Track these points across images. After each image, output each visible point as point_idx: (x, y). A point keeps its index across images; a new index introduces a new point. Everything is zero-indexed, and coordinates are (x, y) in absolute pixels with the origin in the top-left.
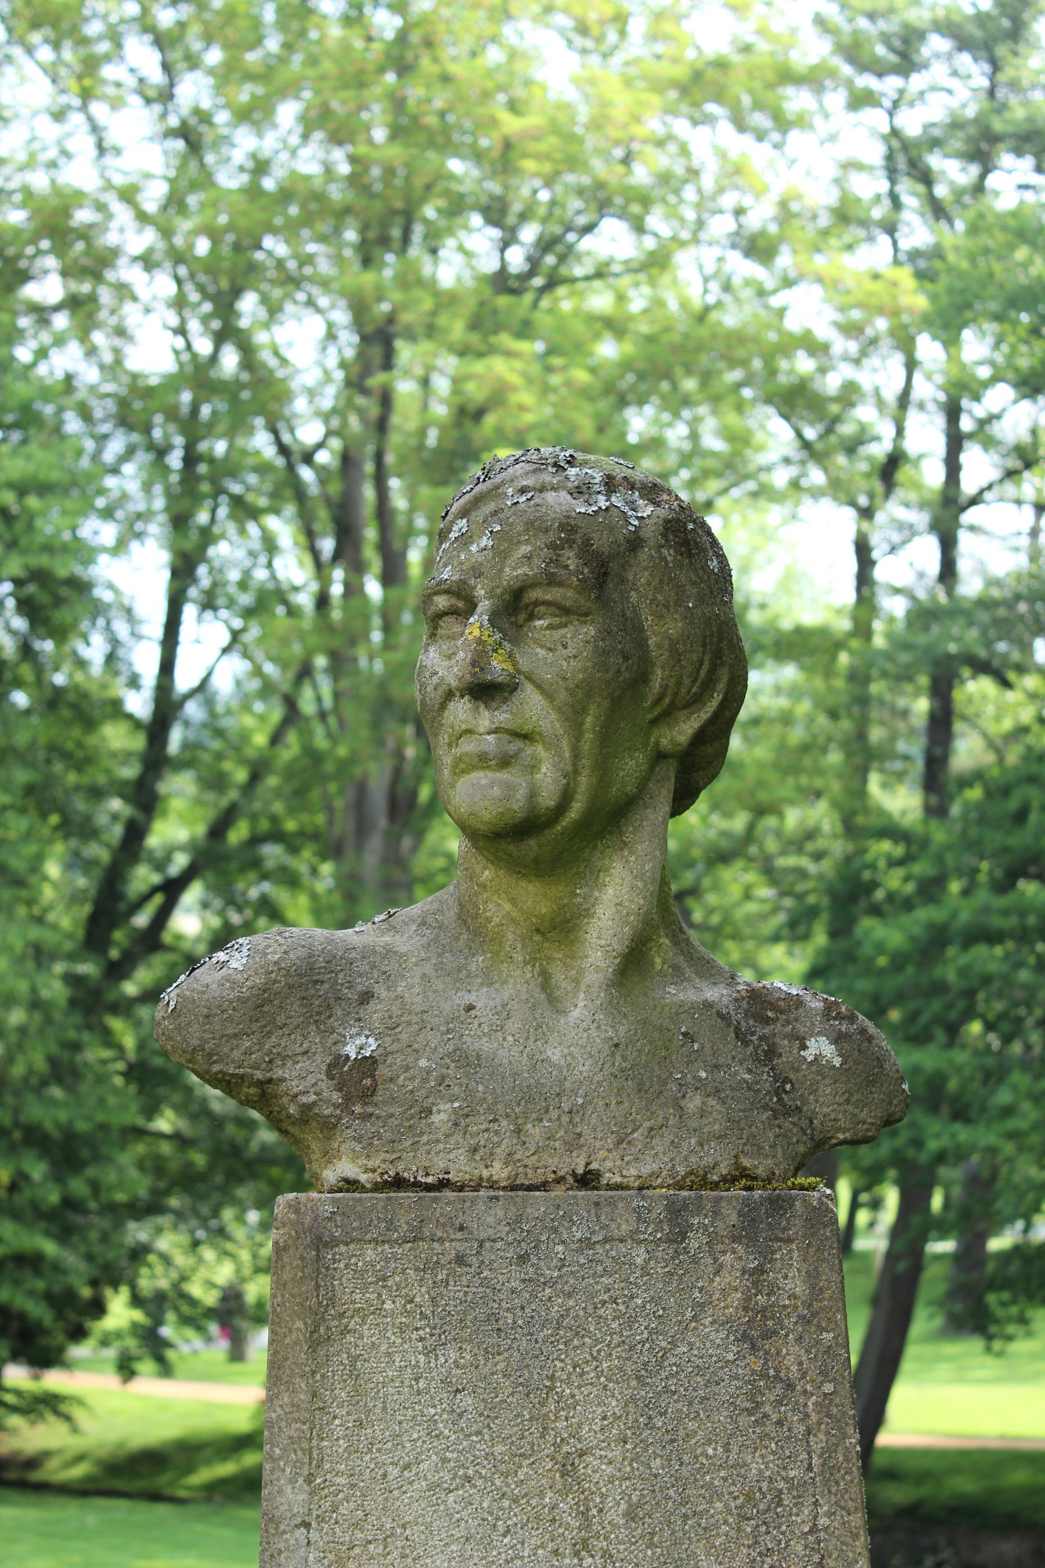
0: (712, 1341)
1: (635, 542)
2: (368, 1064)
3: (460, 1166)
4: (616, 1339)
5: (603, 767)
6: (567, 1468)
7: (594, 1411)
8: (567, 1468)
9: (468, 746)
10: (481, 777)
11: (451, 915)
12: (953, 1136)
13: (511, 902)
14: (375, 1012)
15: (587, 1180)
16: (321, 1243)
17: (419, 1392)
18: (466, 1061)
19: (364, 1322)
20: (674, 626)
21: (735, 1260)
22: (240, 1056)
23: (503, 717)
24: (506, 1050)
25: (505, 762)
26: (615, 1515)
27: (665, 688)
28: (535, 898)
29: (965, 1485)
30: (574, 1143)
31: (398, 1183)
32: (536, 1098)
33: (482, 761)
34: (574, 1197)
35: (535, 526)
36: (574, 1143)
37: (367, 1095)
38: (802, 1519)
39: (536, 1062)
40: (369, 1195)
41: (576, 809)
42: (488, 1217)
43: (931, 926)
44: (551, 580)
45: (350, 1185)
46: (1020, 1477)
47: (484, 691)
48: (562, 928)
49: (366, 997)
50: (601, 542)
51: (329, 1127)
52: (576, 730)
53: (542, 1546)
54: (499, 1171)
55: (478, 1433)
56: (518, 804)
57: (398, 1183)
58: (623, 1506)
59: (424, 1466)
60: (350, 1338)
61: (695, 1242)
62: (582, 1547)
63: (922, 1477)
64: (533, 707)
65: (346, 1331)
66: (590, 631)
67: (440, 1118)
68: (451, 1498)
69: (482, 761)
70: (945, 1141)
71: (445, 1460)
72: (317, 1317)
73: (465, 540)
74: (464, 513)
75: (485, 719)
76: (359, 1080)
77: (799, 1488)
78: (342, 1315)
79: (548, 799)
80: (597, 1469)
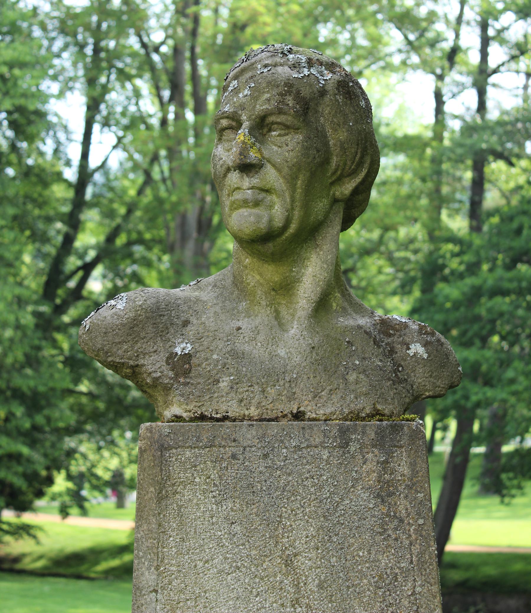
0: (362, 497)
1: (323, 92)
2: (187, 357)
3: (234, 410)
4: (313, 497)
5: (306, 206)
6: (288, 562)
7: (302, 533)
8: (288, 562)
9: (238, 196)
10: (244, 211)
11: (229, 281)
12: (484, 393)
13: (260, 275)
14: (191, 331)
15: (298, 416)
16: (163, 448)
17: (213, 524)
18: (237, 356)
19: (185, 488)
20: (343, 135)
21: (373, 456)
22: (121, 353)
23: (255, 181)
24: (257, 350)
25: (257, 204)
26: (313, 586)
27: (338, 166)
28: (272, 273)
29: (491, 571)
30: (292, 397)
31: (202, 418)
32: (271, 375)
33: (245, 203)
34: (292, 425)
35: (272, 84)
36: (292, 397)
37: (187, 373)
38: (408, 588)
39: (273, 356)
40: (188, 423)
41: (293, 228)
42: (248, 435)
43: (473, 287)
44: (280, 112)
45: (178, 418)
46: (518, 567)
47: (246, 168)
48: (285, 288)
49: (186, 323)
50: (305, 92)
51: (167, 389)
52: (293, 188)
53: (276, 602)
54: (253, 412)
55: (243, 544)
56: (263, 225)
57: (202, 418)
58: (317, 581)
59: (216, 561)
60: (178, 496)
61: (353, 447)
62: (296, 602)
63: (469, 567)
64: (271, 176)
65: (176, 493)
66: (300, 137)
67: (224, 384)
68: (229, 577)
69: (245, 203)
70: (480, 396)
71: (226, 558)
72: (161, 486)
73: (236, 91)
74: (236, 77)
75: (247, 182)
76: (182, 365)
77: (406, 573)
78: (174, 485)
79: (278, 223)
80: (303, 563)
